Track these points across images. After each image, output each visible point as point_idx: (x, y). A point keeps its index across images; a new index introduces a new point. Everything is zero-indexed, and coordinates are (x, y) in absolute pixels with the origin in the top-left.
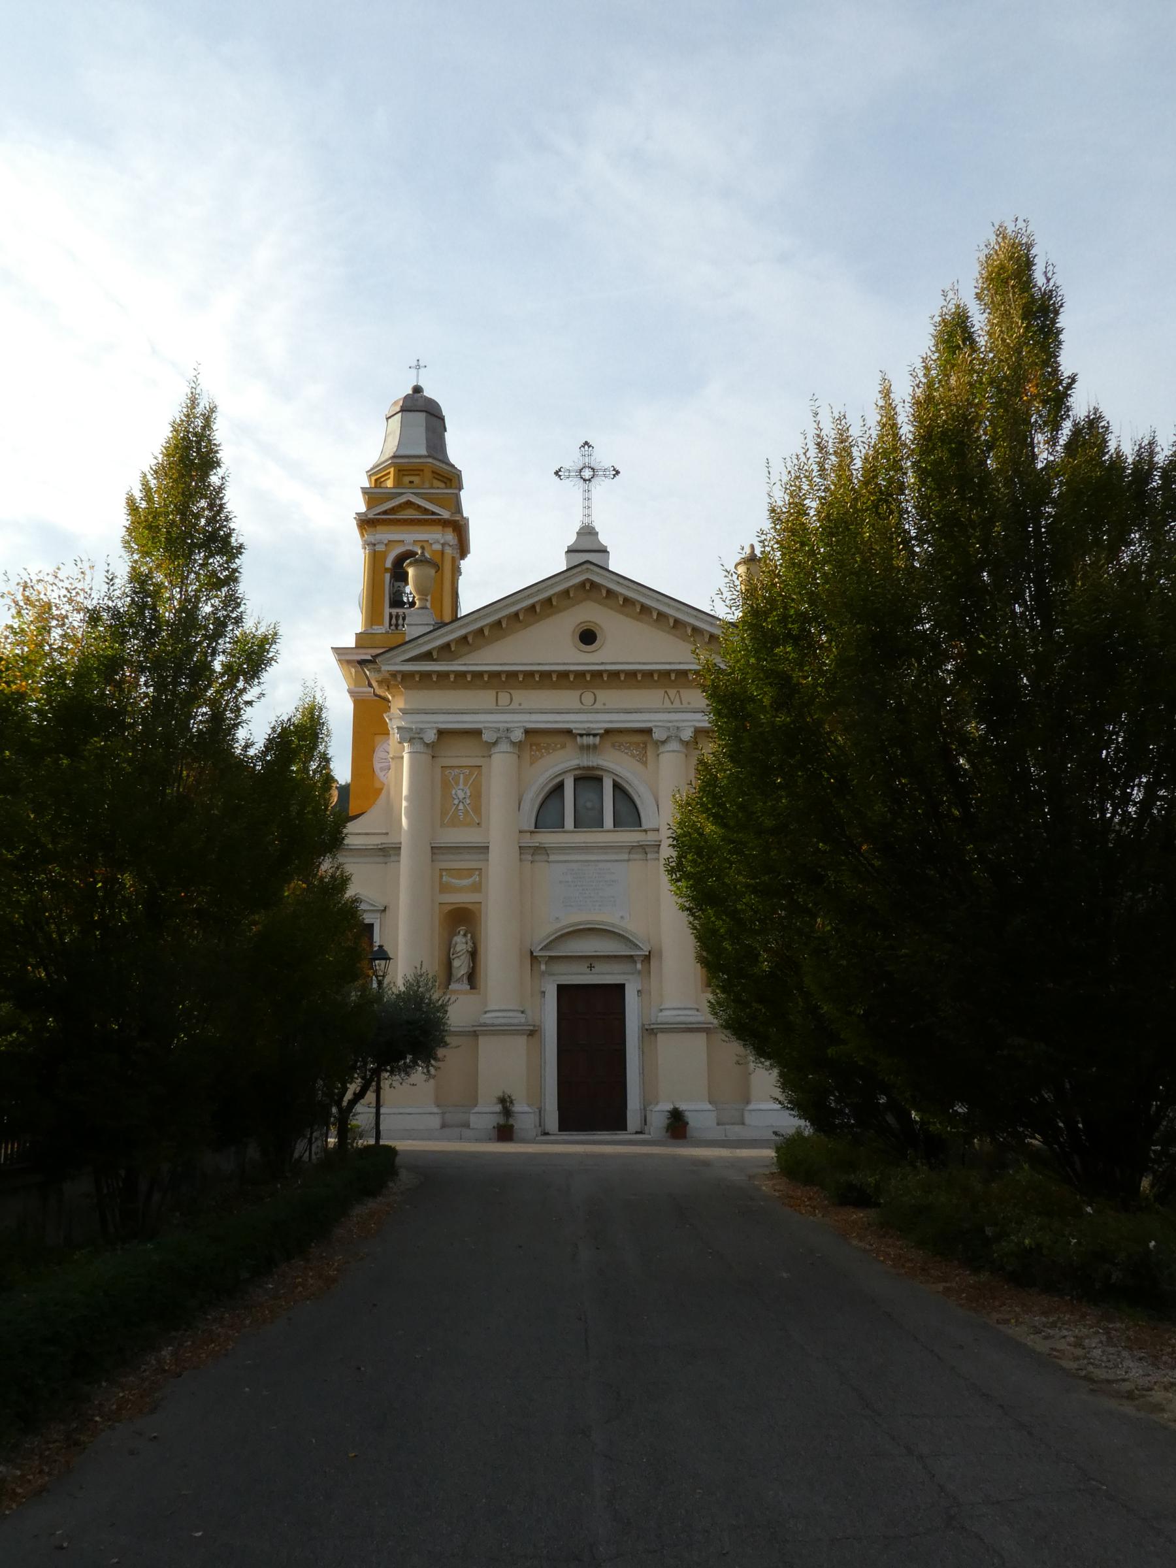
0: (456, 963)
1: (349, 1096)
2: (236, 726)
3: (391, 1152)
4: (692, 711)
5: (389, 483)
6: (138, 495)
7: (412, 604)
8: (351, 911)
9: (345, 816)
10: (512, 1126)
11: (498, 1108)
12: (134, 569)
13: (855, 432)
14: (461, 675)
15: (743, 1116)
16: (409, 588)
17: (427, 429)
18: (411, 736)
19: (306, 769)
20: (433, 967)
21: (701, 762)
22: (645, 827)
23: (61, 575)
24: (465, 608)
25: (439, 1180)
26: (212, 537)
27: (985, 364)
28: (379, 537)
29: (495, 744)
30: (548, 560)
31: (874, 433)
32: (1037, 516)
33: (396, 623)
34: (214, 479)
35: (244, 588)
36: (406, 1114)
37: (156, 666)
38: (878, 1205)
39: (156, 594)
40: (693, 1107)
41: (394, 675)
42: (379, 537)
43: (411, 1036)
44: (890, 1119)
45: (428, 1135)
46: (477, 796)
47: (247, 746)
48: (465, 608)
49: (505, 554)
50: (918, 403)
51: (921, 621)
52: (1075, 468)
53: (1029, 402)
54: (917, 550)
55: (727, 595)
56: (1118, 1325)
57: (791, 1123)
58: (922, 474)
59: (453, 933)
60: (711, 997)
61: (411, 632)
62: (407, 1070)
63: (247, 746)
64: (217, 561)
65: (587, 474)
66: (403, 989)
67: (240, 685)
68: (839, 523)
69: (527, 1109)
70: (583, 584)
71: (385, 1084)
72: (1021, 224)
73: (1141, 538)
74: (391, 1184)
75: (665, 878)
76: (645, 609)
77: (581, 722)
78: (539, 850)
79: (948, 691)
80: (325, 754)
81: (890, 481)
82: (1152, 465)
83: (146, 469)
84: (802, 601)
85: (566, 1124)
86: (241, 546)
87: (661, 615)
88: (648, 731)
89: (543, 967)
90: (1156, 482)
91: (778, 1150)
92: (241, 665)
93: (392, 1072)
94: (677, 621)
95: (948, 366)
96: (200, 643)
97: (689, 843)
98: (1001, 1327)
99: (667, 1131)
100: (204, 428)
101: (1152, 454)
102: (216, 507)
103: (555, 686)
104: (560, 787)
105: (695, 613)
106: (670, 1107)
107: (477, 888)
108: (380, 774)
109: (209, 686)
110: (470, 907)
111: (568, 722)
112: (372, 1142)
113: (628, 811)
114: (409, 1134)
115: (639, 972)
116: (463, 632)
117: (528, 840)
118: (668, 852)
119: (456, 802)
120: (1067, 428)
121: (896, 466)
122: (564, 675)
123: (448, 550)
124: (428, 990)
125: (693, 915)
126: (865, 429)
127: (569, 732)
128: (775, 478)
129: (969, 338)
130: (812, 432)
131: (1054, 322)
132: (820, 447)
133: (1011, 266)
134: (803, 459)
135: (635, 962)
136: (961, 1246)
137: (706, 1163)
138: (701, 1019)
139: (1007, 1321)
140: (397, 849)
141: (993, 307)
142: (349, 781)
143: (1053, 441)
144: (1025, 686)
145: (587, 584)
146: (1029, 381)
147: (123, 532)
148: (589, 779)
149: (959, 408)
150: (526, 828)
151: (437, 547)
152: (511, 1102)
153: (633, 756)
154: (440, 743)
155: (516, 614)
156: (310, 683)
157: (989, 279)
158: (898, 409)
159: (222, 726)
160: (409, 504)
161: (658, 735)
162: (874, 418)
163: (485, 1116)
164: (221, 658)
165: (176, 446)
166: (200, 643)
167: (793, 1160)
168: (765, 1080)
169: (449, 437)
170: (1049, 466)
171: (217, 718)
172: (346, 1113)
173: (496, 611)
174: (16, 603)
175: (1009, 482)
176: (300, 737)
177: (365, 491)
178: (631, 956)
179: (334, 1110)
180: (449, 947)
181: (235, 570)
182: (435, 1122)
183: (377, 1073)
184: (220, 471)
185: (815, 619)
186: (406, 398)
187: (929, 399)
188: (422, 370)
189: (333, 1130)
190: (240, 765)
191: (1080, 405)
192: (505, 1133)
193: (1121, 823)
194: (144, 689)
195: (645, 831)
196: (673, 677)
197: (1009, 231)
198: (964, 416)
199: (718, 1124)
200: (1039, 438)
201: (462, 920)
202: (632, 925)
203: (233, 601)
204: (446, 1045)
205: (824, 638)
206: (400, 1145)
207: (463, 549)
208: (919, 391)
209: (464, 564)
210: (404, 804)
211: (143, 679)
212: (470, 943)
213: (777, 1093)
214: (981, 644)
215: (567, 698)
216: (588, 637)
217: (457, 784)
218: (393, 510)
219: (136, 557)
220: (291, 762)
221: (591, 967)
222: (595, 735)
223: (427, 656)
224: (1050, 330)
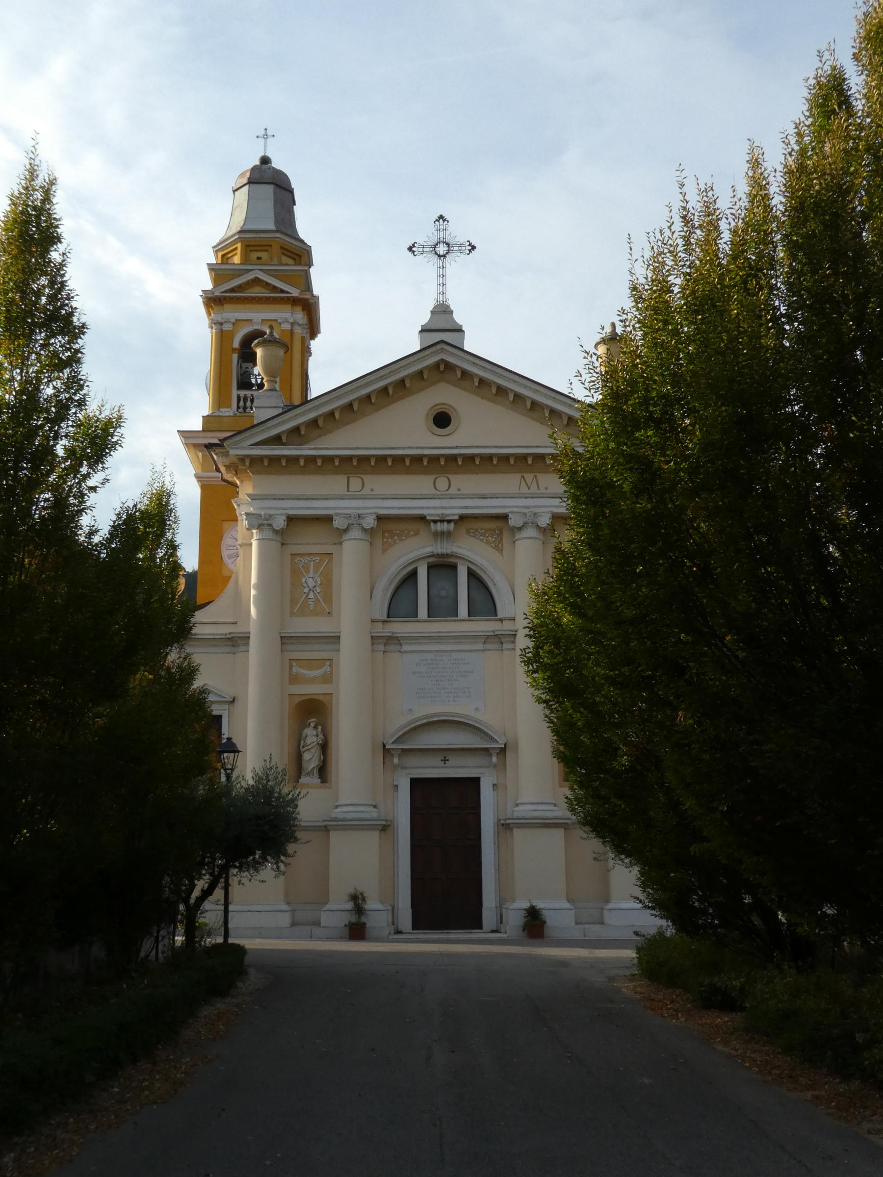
0: (306, 756)
1: (196, 893)
2: (80, 512)
3: (240, 950)
5: (237, 260)
7: (261, 386)
8: (199, 701)
9: (192, 606)
10: (364, 924)
11: (350, 905)
15: (602, 915)
16: (258, 370)
17: (275, 202)
18: (260, 522)
19: (153, 557)
20: (282, 760)
21: (558, 550)
22: (500, 615)
25: (291, 980)
29: (346, 531)
30: (398, 339)
31: (745, 203)
33: (244, 405)
34: (55, 256)
35: (88, 369)
36: (255, 912)
38: (743, 1009)
41: (242, 459)
43: (261, 830)
44: (756, 920)
49: (359, 331)
50: (790, 172)
51: (789, 403)
57: (652, 923)
58: (793, 248)
59: (303, 725)
60: (568, 793)
61: (259, 414)
62: (256, 866)
63: (92, 533)
64: (58, 341)
65: (442, 250)
67: (84, 470)
68: (706, 300)
69: (379, 906)
70: (437, 365)
71: (234, 881)
75: (521, 669)
76: (501, 391)
77: (435, 508)
78: (392, 640)
81: (760, 256)
84: (664, 383)
85: (419, 923)
87: (517, 396)
88: (504, 517)
89: (396, 760)
91: (639, 950)
92: (84, 449)
93: (240, 868)
95: (822, 132)
97: (545, 633)
99: (524, 930)
100: (43, 202)
102: (58, 285)
103: (408, 471)
104: (413, 576)
105: (553, 395)
106: (526, 905)
107: (327, 679)
108: (228, 561)
110: (321, 698)
111: (422, 508)
112: (220, 940)
115: (495, 766)
118: (524, 642)
119: (306, 590)
121: (765, 239)
122: (417, 459)
123: (298, 330)
125: (549, 707)
126: (732, 199)
127: (422, 518)
129: (845, 102)
130: (677, 204)
134: (667, 233)
135: (491, 755)
137: (564, 964)
141: (871, 69)
142: (196, 568)
145: (441, 364)
148: (443, 567)
149: (833, 177)
150: (378, 617)
152: (364, 899)
153: (488, 543)
154: (289, 530)
155: (368, 397)
156: (159, 468)
157: (867, 38)
159: (65, 514)
160: (257, 281)
161: (514, 521)
162: (743, 189)
163: (336, 912)
164: (64, 442)
165: (15, 221)
167: (654, 961)
168: (625, 877)
169: (299, 211)
171: (59, 503)
172: (194, 910)
176: (148, 523)
177: (211, 268)
178: (487, 749)
179: (182, 907)
181: (78, 351)
182: (285, 920)
184: (61, 247)
189: (180, 928)
190: (86, 553)
192: (357, 931)
195: (501, 620)
196: (530, 461)
198: (840, 187)
199: (577, 923)
201: (312, 711)
202: (488, 716)
203: (75, 383)
204: (296, 840)
206: (249, 944)
207: (313, 330)
210: (253, 592)
212: (321, 736)
213: (638, 892)
214: (852, 426)
215: (421, 483)
216: (442, 420)
217: (308, 571)
220: (137, 550)
221: (445, 760)
222: (449, 521)
223: (276, 440)
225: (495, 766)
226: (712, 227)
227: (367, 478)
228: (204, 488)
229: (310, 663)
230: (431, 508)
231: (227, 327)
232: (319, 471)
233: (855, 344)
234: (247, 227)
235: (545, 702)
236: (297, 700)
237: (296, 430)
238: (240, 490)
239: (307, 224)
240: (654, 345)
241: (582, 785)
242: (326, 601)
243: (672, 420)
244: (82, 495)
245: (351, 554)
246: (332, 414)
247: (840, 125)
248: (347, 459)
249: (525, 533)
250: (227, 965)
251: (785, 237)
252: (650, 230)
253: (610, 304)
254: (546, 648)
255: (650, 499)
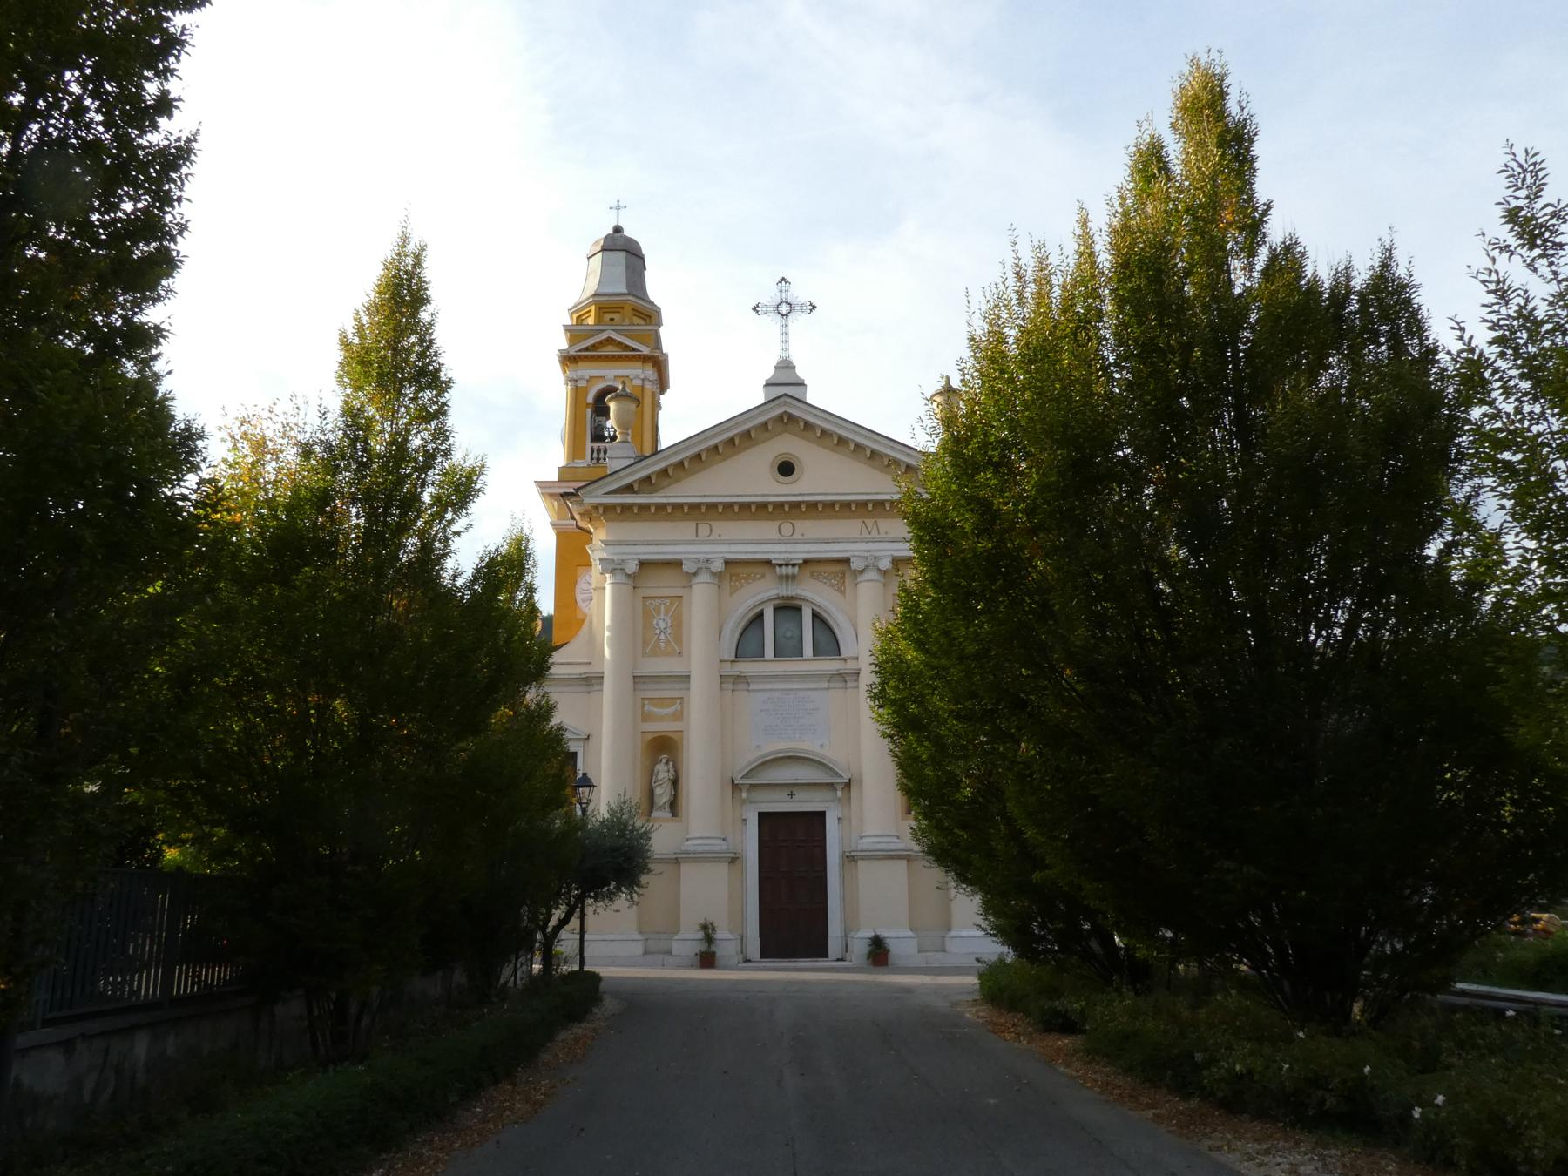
0: (658, 791)
1: (553, 922)
2: (445, 555)
3: (595, 978)
4: (894, 540)
5: (591, 321)
6: (350, 331)
7: (614, 438)
8: (556, 739)
9: (548, 649)
10: (714, 953)
11: (701, 935)
12: (346, 402)
13: (1054, 260)
14: (661, 507)
15: (943, 943)
16: (611, 422)
17: (627, 267)
18: (612, 567)
19: (513, 599)
20: (636, 796)
21: (903, 589)
23: (276, 409)
24: (665, 442)
25: (644, 1006)
26: (422, 372)
27: (1181, 192)
28: (580, 373)
29: (695, 574)
30: (747, 395)
31: (1072, 261)
32: (1236, 339)
33: (598, 457)
34: (424, 316)
35: (453, 421)
36: (609, 940)
37: (367, 499)
38: (1083, 1032)
39: (367, 428)
40: (893, 934)
41: (596, 507)
42: (580, 373)
43: (615, 863)
44: (1094, 945)
45: (630, 962)
46: (678, 625)
47: (455, 576)
48: (665, 442)
49: (703, 392)
50: (1114, 231)
51: (1121, 446)
52: (1273, 293)
53: (1225, 229)
54: (1117, 376)
55: (928, 423)
56: (1333, 1152)
57: (995, 950)
58: (1120, 302)
59: (655, 762)
60: (913, 824)
61: (612, 465)
62: (611, 896)
63: (455, 576)
64: (426, 395)
65: (785, 309)
66: (607, 816)
67: (449, 516)
68: (1039, 352)
70: (781, 417)
71: (589, 911)
72: (1214, 55)
73: (1339, 361)
74: (596, 1010)
75: (865, 705)
76: (842, 441)
78: (741, 679)
79: (1148, 516)
80: (531, 584)
81: (1088, 309)
82: (1349, 290)
83: (359, 307)
84: (1001, 429)
85: (766, 953)
86: (450, 381)
87: (858, 446)
88: (847, 561)
89: (744, 795)
90: (1354, 305)
91: (980, 976)
92: (449, 496)
93: (596, 899)
94: (873, 452)
95: (1143, 195)
96: (411, 474)
97: (891, 668)
98: (1214, 1154)
100: (414, 266)
101: (1348, 278)
102: (426, 343)
103: (754, 517)
106: (871, 934)
107: (678, 716)
108: (582, 605)
109: (418, 517)
112: (576, 968)
113: (828, 640)
114: (614, 961)
115: (840, 800)
116: (663, 465)
117: (729, 669)
118: (868, 678)
120: (1263, 255)
121: (1094, 293)
122: (763, 506)
123: (648, 386)
124: (631, 817)
125: (893, 742)
126: (1064, 258)
127: (768, 562)
128: (974, 306)
129: (1164, 167)
130: (1010, 262)
131: (1248, 150)
132: (1019, 276)
133: (1205, 96)
134: (1002, 288)
136: (1168, 1072)
137: (908, 990)
138: (901, 846)
139: (1219, 1148)
140: (600, 678)
141: (1187, 135)
142: (552, 612)
143: (1249, 267)
144: (1226, 510)
145: (785, 417)
146: (1225, 208)
147: (336, 367)
148: (788, 609)
149: (1156, 236)
151: (637, 382)
153: (831, 585)
154: (643, 574)
155: (716, 447)
156: (518, 515)
157: (1184, 108)
158: (1096, 238)
159: (430, 558)
160: (610, 341)
161: (855, 565)
162: (1071, 246)
163: (687, 942)
164: (431, 489)
165: (388, 285)
166: (411, 474)
167: (998, 989)
168: (967, 907)
169: (649, 275)
170: (1248, 290)
171: (426, 548)
172: (550, 939)
173: (695, 445)
174: (232, 437)
175: (1206, 308)
176: (507, 568)
177: (567, 329)
178: (832, 784)
179: (539, 936)
180: (651, 774)
181: (444, 404)
182: (638, 949)
183: (581, 899)
184: (430, 308)
185: (1015, 445)
186: (606, 238)
187: (1126, 228)
188: (622, 211)
189: (538, 957)
190: (451, 593)
191: (1276, 231)
192: (707, 960)
193: (1326, 644)
194: (354, 520)
196: (870, 507)
197: (1202, 62)
198: (1162, 245)
200: (1235, 264)
201: (663, 747)
202: (833, 752)
203: (442, 434)
204: (649, 871)
205: (1023, 464)
206: (604, 972)
207: (663, 384)
208: (1115, 222)
209: (664, 399)
210: (607, 634)
211: (354, 510)
213: (980, 920)
214: (1181, 468)
215: (767, 529)
216: (786, 469)
217: (659, 613)
218: (594, 347)
219: (349, 391)
220: (497, 591)
221: (792, 795)
223: (629, 489)
224: (1245, 158)
225: (840, 800)
226: (1044, 281)
227: (715, 524)
228: (558, 535)
229: (661, 702)
230: (776, 552)
231: (582, 384)
232: (669, 518)
233: (1181, 391)
234: (601, 291)
235: (890, 736)
236: (650, 736)
237: (647, 479)
238: (594, 537)
239: (657, 287)
240: (993, 392)
241: (926, 817)
242: (677, 641)
243: (1010, 463)
244: (447, 539)
245: (700, 599)
246: (681, 463)
247: (1160, 188)
248: (695, 507)
249: (866, 576)
250: (584, 990)
251: (1112, 291)
252: (986, 285)
253: (947, 356)
254: (892, 683)
255: (990, 538)
